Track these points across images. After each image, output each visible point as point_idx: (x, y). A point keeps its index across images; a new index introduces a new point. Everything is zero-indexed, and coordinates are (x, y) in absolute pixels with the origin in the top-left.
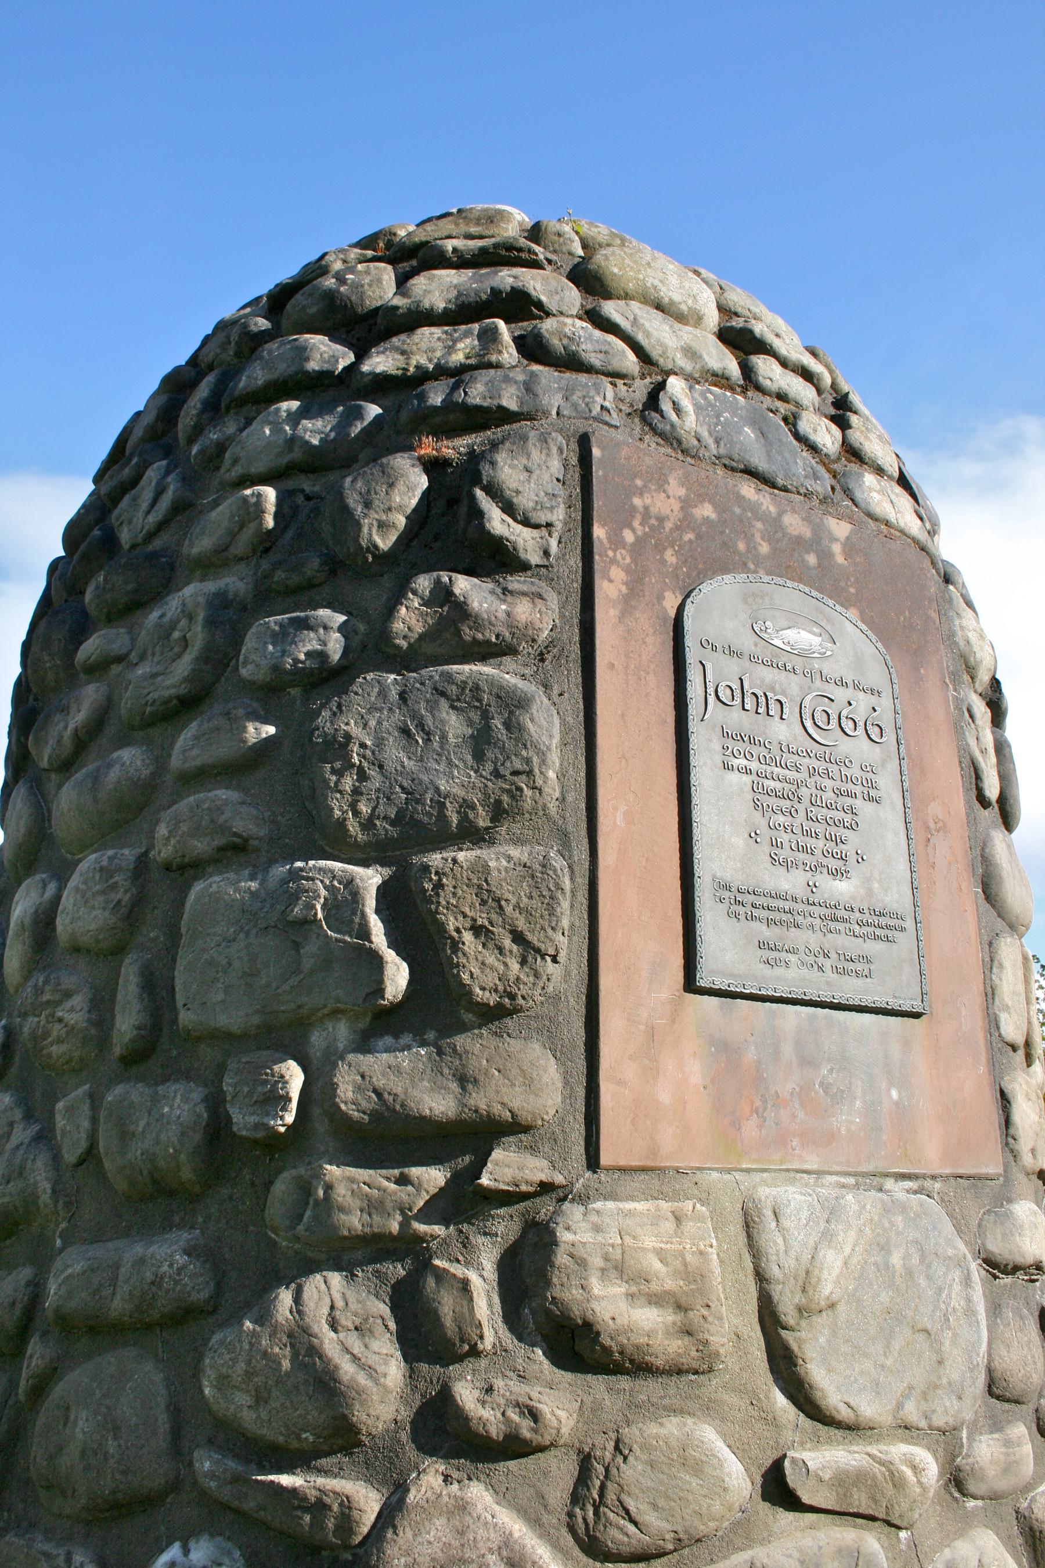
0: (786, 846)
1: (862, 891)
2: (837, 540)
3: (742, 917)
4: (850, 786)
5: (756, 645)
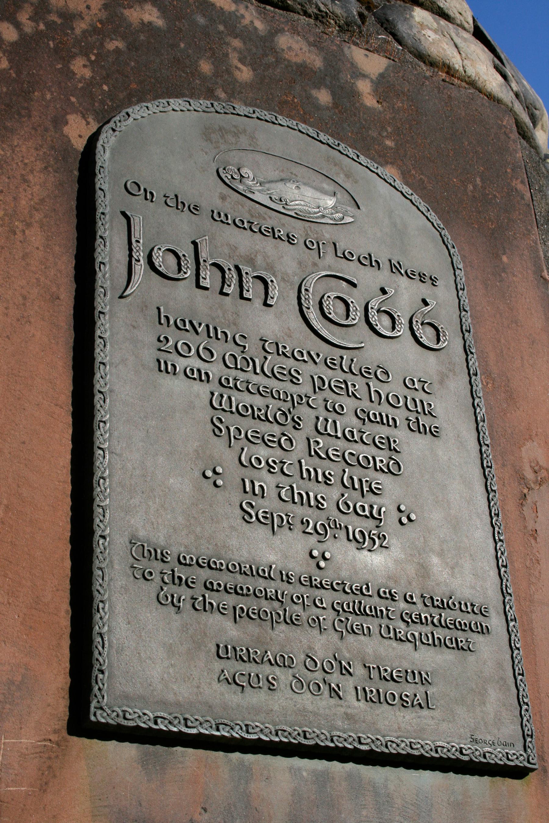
0: (271, 492)
1: (411, 570)
2: (364, 76)
3: (186, 606)
4: (385, 409)
5: (223, 198)
